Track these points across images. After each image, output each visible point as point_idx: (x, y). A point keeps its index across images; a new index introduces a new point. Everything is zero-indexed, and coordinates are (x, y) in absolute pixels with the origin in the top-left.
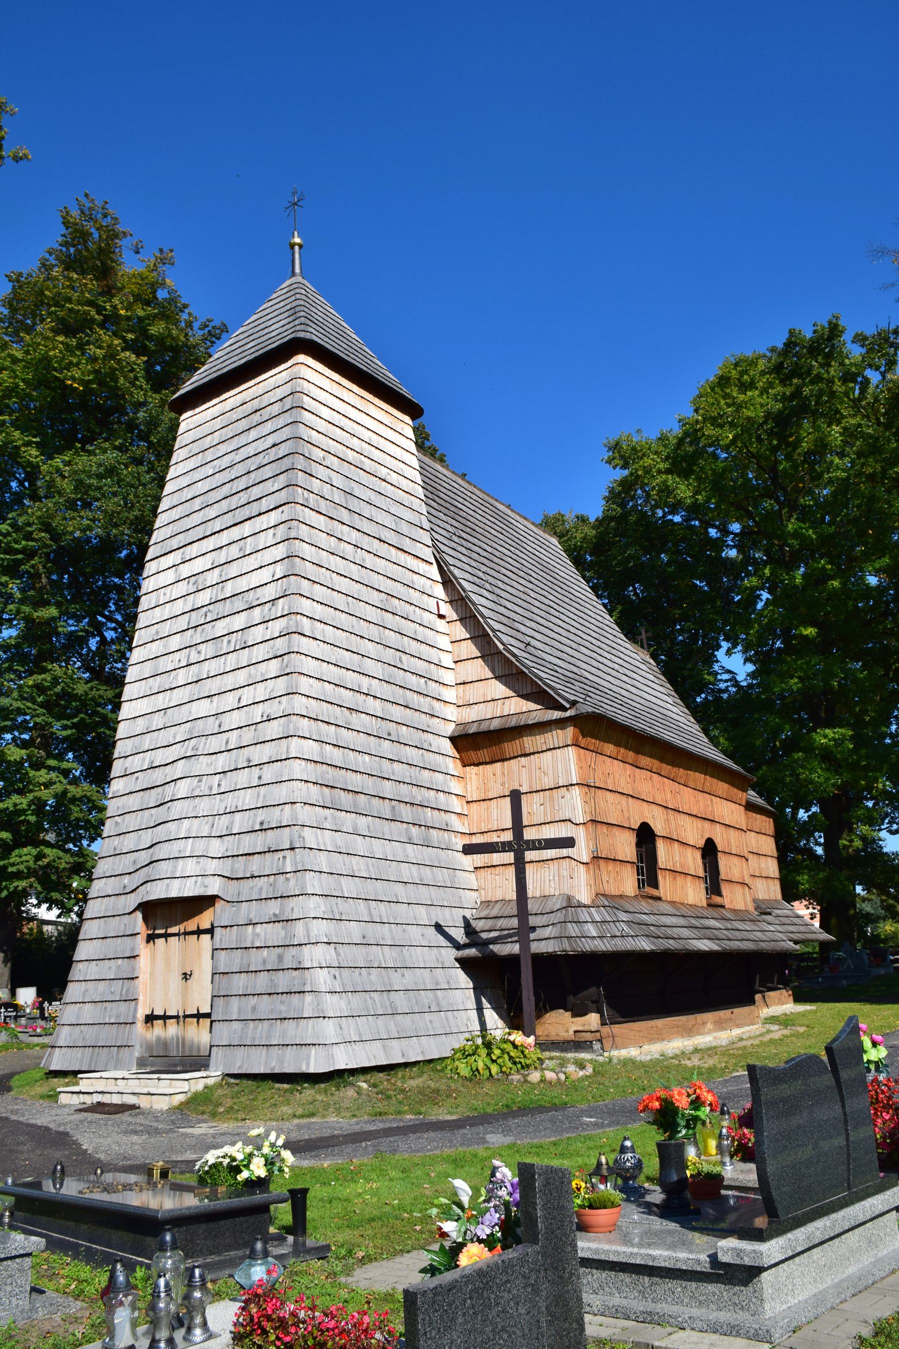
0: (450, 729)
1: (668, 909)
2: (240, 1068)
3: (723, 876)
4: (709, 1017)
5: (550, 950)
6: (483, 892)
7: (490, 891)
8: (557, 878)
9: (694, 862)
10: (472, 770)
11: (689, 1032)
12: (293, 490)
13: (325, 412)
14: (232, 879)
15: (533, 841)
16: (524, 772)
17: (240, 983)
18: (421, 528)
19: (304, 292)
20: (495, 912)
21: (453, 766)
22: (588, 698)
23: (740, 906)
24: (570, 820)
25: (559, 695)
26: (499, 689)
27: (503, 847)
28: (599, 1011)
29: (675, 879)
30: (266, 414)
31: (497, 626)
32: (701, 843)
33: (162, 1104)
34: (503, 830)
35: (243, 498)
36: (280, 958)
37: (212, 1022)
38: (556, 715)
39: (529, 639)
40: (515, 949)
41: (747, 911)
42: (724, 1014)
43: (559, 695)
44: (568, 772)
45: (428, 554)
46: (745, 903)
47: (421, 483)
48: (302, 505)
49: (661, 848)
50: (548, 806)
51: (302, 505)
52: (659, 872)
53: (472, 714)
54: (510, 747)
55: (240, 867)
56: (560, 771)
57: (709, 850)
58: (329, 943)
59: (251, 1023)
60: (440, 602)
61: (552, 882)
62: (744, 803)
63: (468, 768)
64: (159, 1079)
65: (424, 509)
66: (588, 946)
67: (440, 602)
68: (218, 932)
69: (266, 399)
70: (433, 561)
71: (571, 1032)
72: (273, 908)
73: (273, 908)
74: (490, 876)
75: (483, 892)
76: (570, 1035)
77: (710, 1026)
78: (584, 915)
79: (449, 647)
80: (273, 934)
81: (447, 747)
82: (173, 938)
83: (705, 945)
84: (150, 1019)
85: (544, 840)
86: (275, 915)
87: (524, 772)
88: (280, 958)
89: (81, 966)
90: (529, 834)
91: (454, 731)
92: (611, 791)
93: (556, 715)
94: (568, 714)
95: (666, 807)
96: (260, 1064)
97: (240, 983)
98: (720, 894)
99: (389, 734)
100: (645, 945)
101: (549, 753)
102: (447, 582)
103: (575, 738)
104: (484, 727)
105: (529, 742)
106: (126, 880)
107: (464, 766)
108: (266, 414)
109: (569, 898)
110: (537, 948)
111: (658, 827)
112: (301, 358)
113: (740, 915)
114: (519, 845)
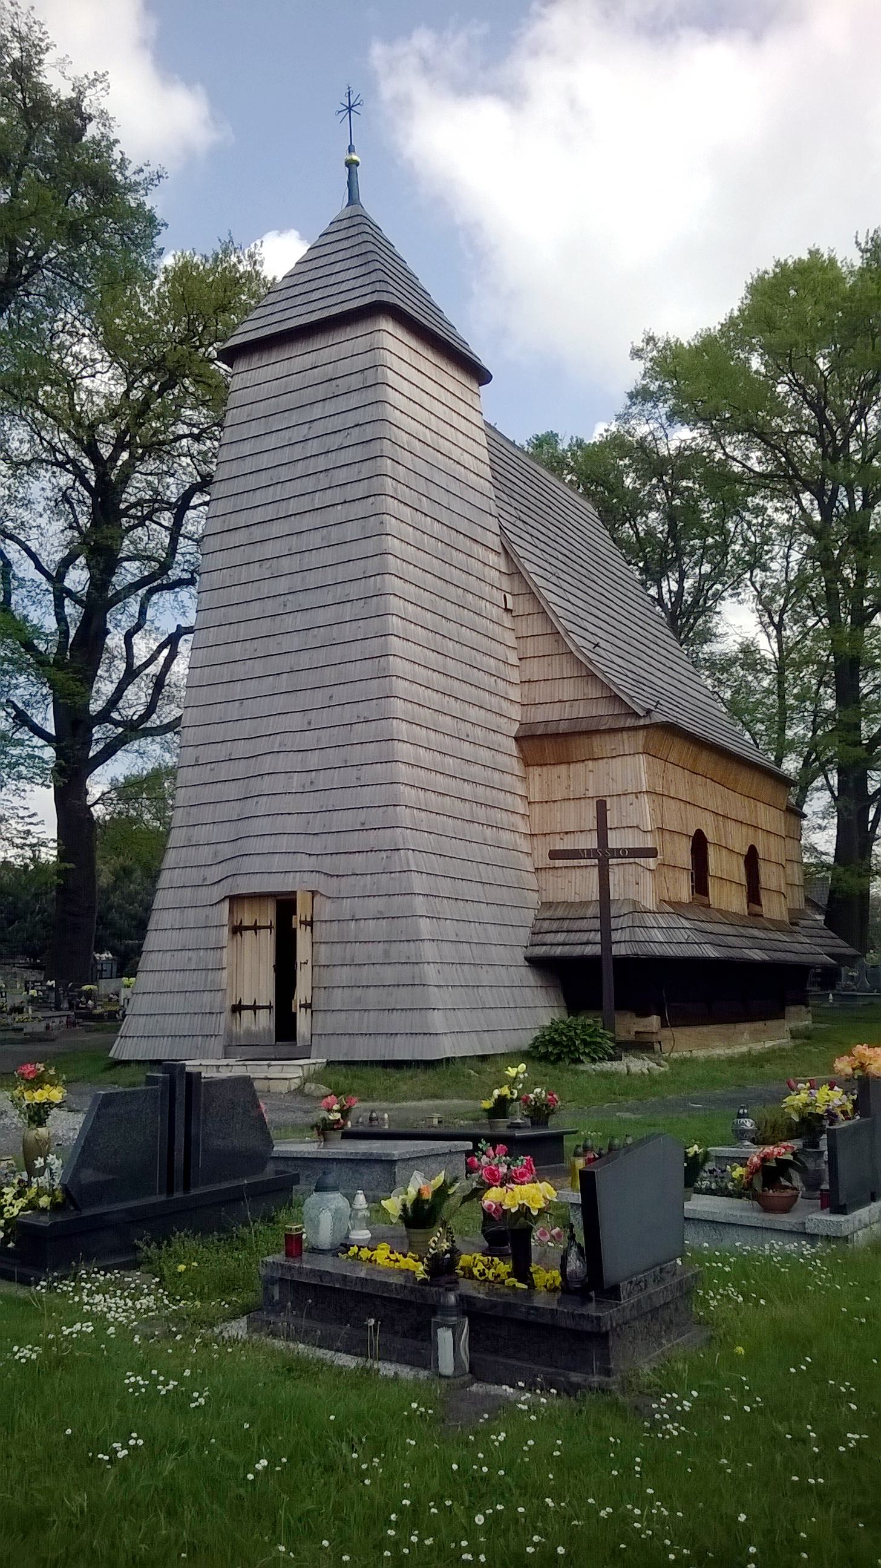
0: (514, 729)
1: (718, 917)
2: (346, 1054)
3: (763, 884)
4: (745, 1028)
5: (623, 953)
6: (544, 893)
7: (551, 892)
8: (622, 884)
9: (739, 872)
10: (536, 771)
11: (729, 1041)
12: (383, 479)
13: (405, 387)
14: (332, 876)
15: (618, 850)
16: (591, 777)
17: (343, 975)
18: (491, 514)
19: (373, 240)
20: (560, 913)
21: (517, 767)
22: (659, 706)
23: (776, 916)
24: (637, 827)
25: (634, 702)
27: (590, 854)
28: (661, 1014)
29: (722, 886)
30: (343, 385)
31: (570, 627)
32: (745, 851)
33: (283, 1087)
34: (567, 833)
35: (324, 481)
36: (386, 953)
37: (312, 1012)
38: (630, 722)
39: (599, 640)
40: (594, 950)
41: (782, 921)
42: (759, 1025)
43: (634, 702)
44: (638, 779)
45: (494, 541)
46: (781, 913)
47: (488, 462)
48: (392, 497)
49: (712, 853)
50: (615, 812)
51: (392, 497)
52: (709, 878)
53: (540, 715)
54: (579, 747)
56: (629, 779)
57: (752, 859)
58: (433, 940)
59: (357, 1014)
60: (507, 595)
61: (617, 888)
62: (784, 808)
63: (531, 768)
64: (269, 1065)
65: (491, 492)
66: (657, 950)
67: (507, 595)
68: (317, 926)
69: (344, 367)
70: (500, 550)
71: (633, 1033)
74: (551, 878)
75: (544, 893)
76: (632, 1037)
77: (746, 1036)
78: (650, 920)
79: (512, 642)
81: (512, 746)
82: (248, 932)
83: (757, 955)
84: (237, 1009)
85: (628, 849)
86: (381, 912)
87: (591, 777)
88: (386, 953)
89: (153, 956)
90: (615, 841)
91: (518, 731)
92: (673, 798)
94: (642, 722)
95: (717, 814)
96: (363, 1051)
97: (343, 975)
98: (759, 904)
99: (468, 736)
100: (711, 952)
101: (620, 759)
102: (515, 572)
103: (646, 745)
104: (552, 729)
105: (599, 744)
107: (527, 765)
108: (343, 385)
109: (635, 903)
110: (619, 950)
111: (710, 836)
112: (387, 325)
113: (777, 926)
114: (604, 853)
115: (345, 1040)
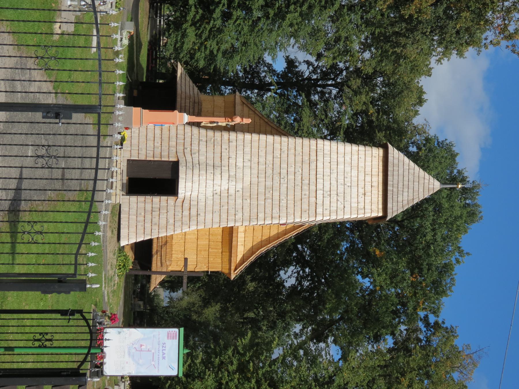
26: (249, 246)
38: (233, 268)
40: (154, 268)
53: (241, 236)
54: (227, 249)
55: (186, 205)
72: (171, 221)
73: (171, 221)
80: (163, 222)
93: (233, 268)
94: (232, 272)
106: (189, 149)
115: (127, 209)
